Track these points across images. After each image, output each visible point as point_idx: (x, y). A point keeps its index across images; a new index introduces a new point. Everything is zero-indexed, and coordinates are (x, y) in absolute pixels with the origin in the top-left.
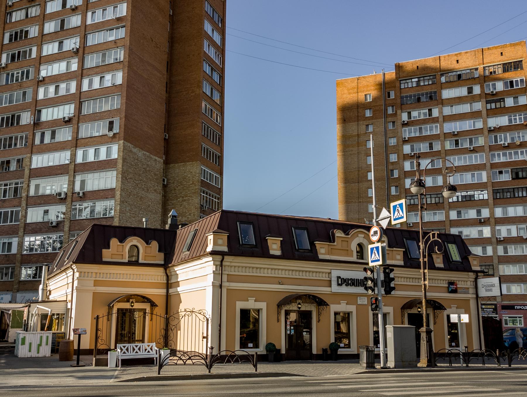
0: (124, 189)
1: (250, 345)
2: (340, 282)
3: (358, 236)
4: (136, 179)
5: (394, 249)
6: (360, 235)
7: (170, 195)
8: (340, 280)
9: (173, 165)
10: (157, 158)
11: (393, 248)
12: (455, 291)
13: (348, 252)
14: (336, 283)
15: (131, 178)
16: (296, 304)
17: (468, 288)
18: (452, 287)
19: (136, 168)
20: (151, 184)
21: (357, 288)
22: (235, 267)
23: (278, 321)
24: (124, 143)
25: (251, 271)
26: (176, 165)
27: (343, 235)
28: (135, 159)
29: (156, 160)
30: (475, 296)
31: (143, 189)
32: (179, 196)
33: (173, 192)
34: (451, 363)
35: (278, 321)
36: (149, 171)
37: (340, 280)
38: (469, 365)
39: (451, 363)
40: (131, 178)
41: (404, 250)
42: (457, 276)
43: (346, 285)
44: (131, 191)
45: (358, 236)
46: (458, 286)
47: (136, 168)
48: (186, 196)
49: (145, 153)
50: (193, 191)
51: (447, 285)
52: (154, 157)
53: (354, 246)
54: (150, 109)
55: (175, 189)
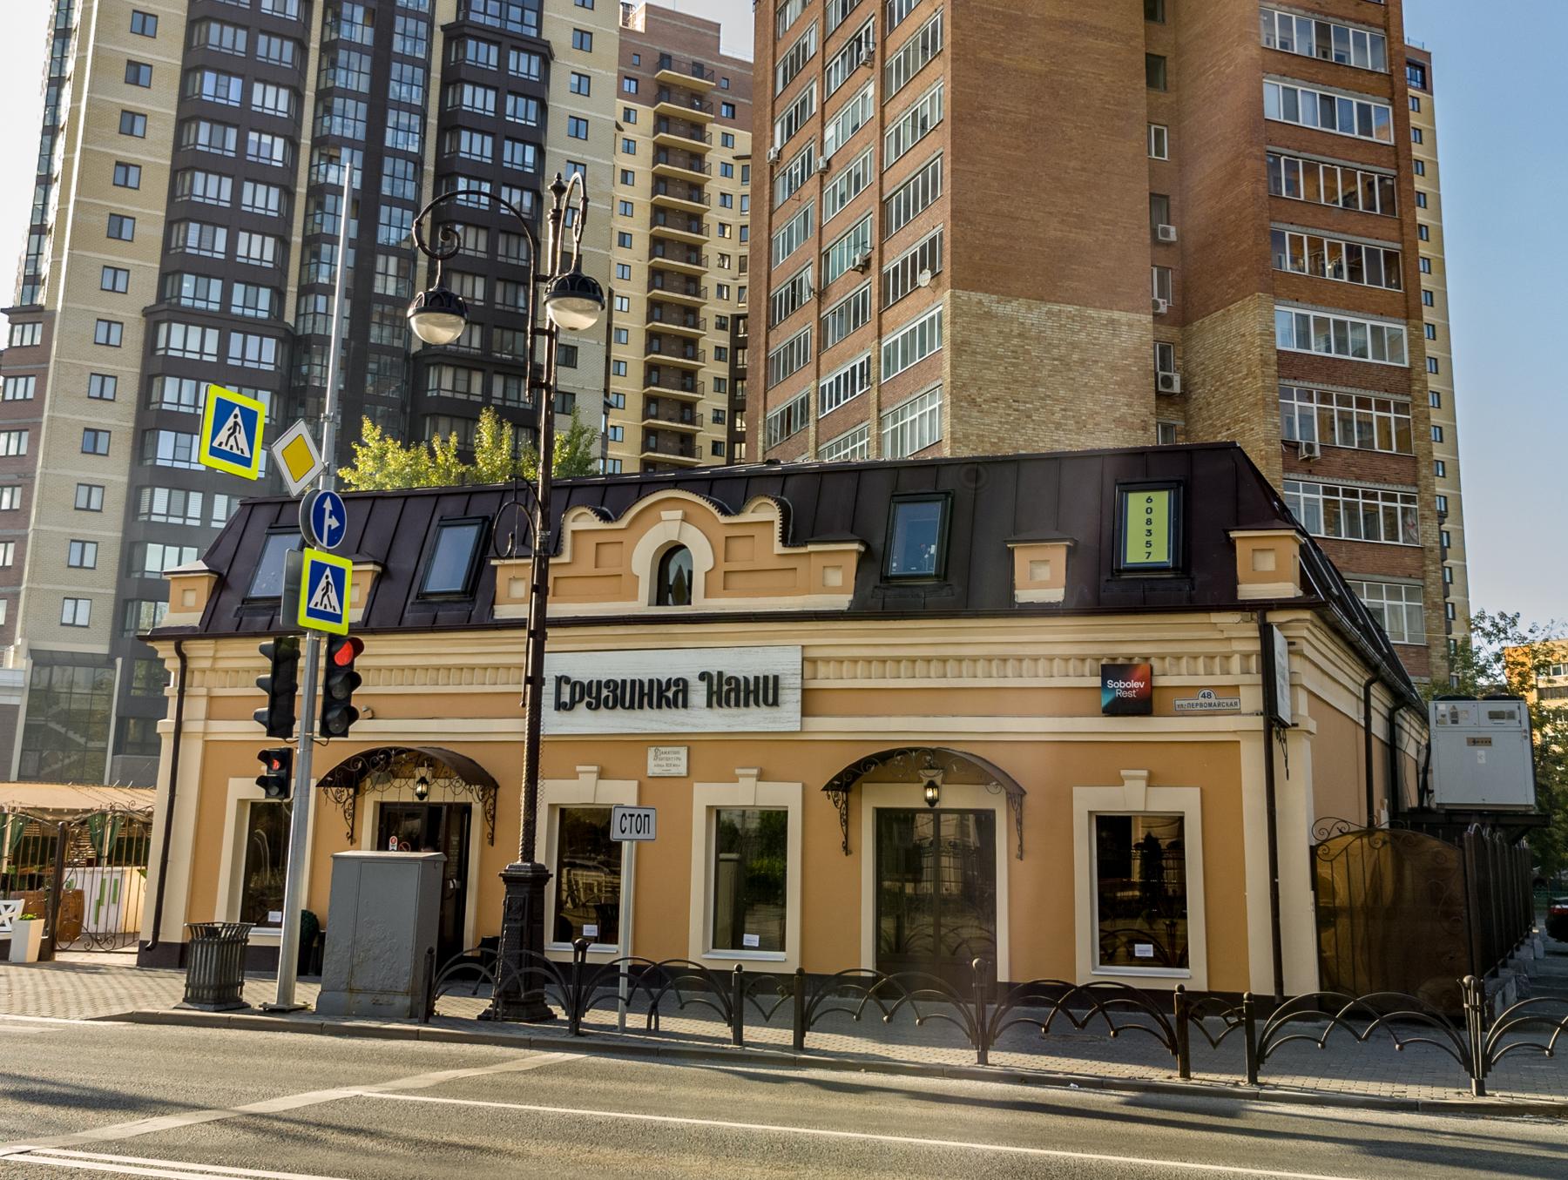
0: (966, 436)
1: (1144, 950)
2: (566, 698)
3: (660, 520)
4: (1021, 396)
5: (811, 548)
6: (665, 515)
7: (1199, 427)
8: (566, 689)
9: (1197, 323)
10: (1116, 315)
11: (805, 544)
12: (1142, 706)
13: (621, 582)
14: (553, 703)
15: (996, 400)
16: (918, 787)
17: (1237, 687)
18: (1119, 687)
19: (1014, 365)
20: (1096, 402)
21: (637, 712)
22: (990, 660)
23: (847, 849)
24: (952, 296)
25: (1201, 669)
26: (1207, 320)
27: (597, 524)
28: (1008, 337)
29: (1112, 321)
30: (1258, 723)
31: (1058, 426)
32: (1218, 423)
33: (1205, 414)
34: (654, 1011)
35: (847, 849)
36: (1082, 362)
37: (566, 689)
38: (667, 1023)
39: (803, 1025)
40: (996, 400)
41: (862, 549)
42: (1156, 635)
43: (589, 705)
44: (1002, 439)
45: (660, 520)
46: (1160, 681)
47: (1014, 365)
48: (1236, 422)
49: (1056, 308)
50: (1251, 399)
51: (1096, 682)
52: (1105, 314)
53: (642, 561)
54: (1072, 164)
55: (1209, 404)
